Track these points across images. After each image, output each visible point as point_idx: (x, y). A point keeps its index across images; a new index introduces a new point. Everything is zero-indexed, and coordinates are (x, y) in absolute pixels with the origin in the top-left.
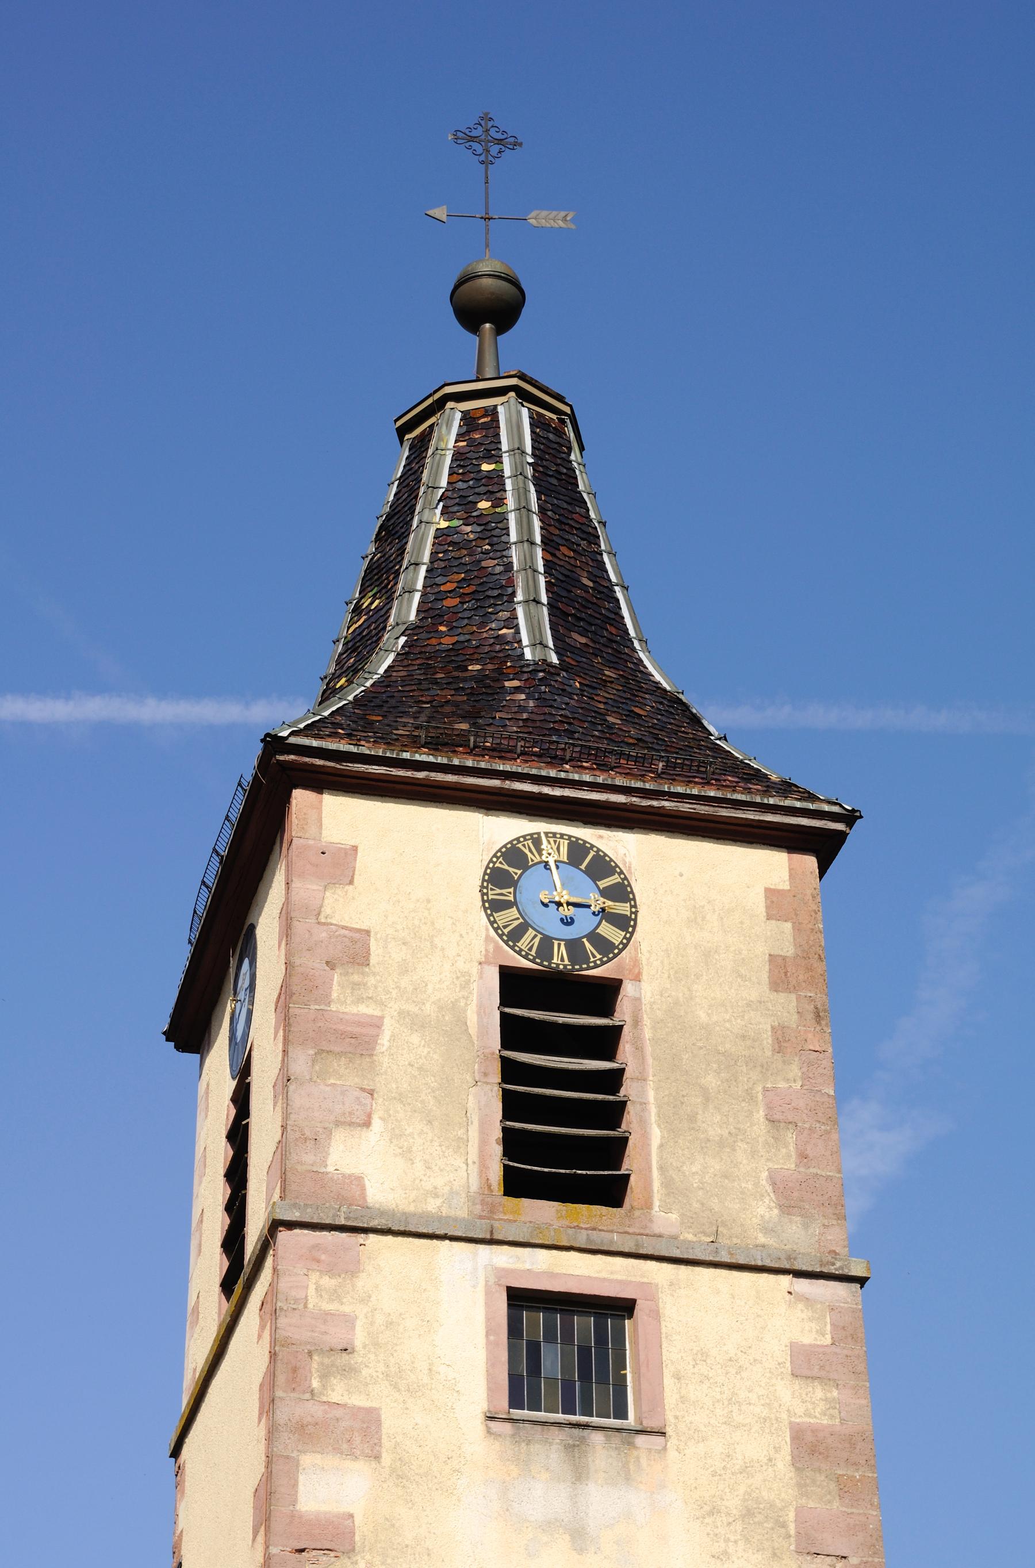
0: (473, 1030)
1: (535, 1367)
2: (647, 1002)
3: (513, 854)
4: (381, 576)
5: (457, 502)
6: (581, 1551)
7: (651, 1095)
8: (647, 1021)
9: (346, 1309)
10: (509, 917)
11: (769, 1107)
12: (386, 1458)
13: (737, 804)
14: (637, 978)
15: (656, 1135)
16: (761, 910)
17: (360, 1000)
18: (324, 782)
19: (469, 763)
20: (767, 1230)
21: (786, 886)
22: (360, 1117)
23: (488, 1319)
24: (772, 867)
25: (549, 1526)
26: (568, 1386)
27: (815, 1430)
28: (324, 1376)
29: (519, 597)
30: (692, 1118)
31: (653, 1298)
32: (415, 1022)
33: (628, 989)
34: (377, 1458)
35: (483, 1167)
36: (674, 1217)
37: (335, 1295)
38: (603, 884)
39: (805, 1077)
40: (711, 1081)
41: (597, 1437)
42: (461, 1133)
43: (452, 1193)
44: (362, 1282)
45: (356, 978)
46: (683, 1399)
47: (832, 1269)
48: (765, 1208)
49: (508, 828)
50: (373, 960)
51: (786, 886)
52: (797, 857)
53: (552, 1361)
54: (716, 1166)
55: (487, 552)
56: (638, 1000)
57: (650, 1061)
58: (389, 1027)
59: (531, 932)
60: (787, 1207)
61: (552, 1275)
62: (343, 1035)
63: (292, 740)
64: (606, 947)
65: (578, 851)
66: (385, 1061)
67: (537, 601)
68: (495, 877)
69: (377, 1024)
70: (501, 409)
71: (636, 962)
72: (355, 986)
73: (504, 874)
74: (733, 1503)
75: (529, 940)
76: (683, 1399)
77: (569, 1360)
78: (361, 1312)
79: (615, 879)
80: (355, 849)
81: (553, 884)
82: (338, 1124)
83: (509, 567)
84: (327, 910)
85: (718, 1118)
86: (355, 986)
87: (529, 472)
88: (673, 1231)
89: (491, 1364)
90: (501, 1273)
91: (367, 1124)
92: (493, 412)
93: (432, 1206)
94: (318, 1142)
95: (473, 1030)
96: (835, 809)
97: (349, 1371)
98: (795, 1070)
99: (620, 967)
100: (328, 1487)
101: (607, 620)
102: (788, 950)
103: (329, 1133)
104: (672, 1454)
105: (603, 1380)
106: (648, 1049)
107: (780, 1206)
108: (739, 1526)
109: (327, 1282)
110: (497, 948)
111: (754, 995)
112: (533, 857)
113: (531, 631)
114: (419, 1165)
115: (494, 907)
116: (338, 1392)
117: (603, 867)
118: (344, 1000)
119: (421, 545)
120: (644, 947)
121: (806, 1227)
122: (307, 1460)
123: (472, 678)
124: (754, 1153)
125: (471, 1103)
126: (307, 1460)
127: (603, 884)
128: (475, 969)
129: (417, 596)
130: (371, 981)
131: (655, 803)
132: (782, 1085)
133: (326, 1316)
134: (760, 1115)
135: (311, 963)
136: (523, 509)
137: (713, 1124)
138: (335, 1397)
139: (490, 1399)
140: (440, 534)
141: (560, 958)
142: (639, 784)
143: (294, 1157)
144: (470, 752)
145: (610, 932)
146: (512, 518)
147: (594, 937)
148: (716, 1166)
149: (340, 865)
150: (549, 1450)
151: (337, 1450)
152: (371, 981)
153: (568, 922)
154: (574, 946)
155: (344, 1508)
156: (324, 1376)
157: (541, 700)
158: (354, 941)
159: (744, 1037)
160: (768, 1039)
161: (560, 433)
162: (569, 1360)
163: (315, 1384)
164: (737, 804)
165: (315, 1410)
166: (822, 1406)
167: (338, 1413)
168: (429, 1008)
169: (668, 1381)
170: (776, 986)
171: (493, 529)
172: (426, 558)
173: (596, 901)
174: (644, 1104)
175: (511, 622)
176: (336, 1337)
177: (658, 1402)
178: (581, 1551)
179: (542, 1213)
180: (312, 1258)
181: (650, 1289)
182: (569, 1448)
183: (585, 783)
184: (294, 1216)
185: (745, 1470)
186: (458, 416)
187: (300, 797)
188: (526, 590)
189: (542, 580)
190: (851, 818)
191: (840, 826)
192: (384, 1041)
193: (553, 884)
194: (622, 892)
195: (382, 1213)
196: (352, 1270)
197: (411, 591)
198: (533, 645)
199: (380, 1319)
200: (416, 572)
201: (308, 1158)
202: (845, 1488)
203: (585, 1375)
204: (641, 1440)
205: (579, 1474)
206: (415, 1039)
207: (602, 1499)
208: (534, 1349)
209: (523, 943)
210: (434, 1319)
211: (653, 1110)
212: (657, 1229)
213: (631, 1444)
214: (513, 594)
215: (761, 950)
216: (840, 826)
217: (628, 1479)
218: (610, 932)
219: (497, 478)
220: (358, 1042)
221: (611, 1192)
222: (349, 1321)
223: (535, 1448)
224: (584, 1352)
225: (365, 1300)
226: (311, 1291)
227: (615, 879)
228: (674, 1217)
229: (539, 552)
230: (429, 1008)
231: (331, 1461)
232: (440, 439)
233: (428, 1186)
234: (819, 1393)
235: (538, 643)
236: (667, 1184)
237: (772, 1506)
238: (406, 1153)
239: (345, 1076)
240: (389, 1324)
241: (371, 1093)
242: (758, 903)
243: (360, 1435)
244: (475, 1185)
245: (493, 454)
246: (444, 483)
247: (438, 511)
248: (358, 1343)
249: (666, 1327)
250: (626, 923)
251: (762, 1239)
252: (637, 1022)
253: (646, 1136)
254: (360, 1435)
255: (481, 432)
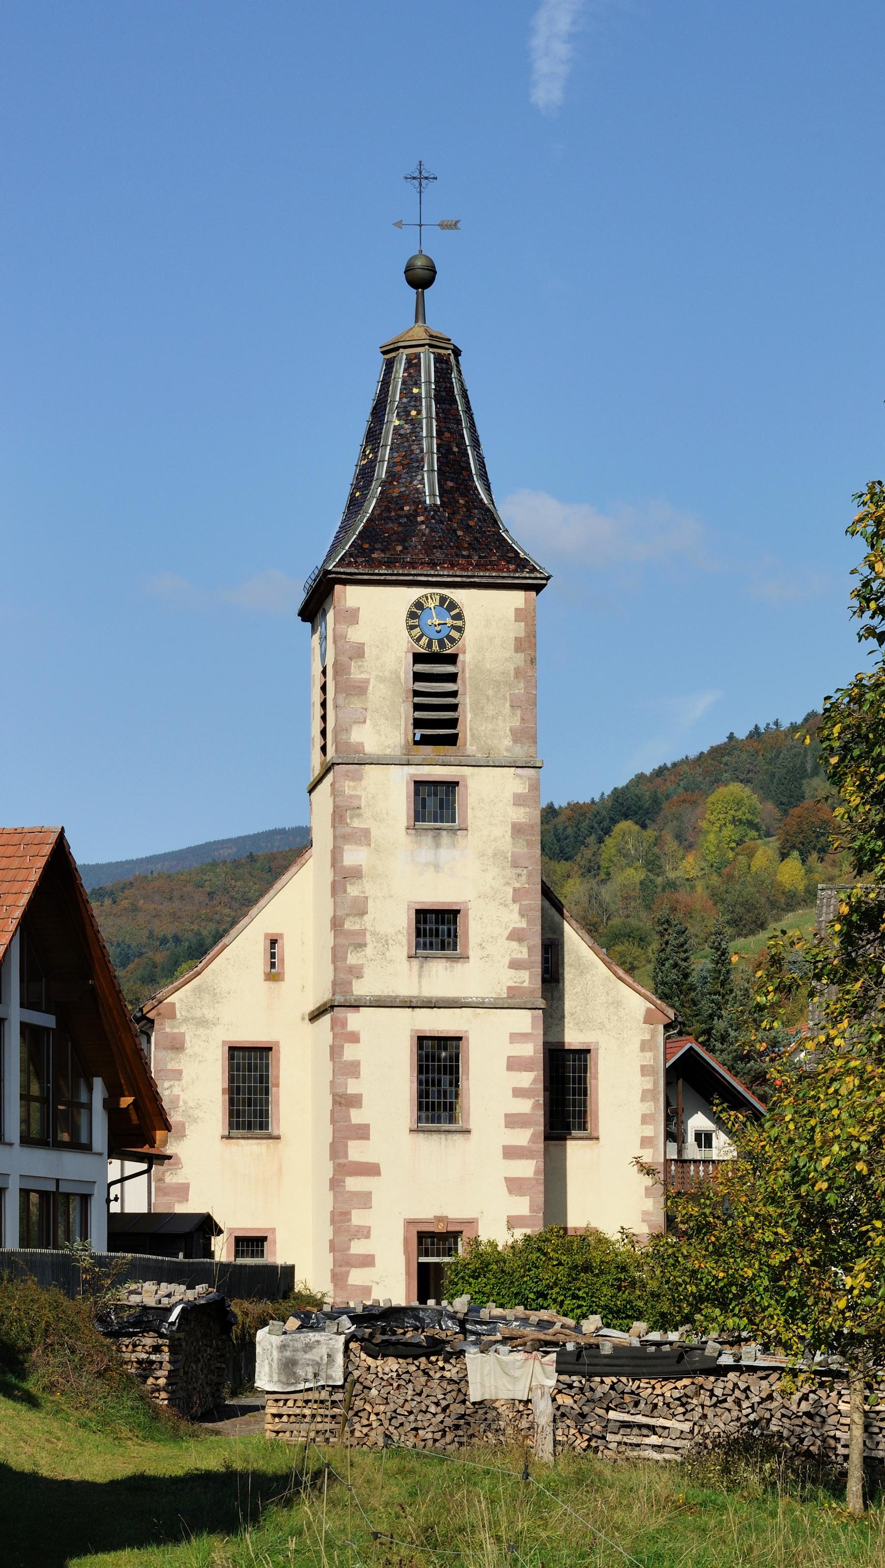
0: (403, 681)
1: (424, 807)
2: (468, 659)
3: (418, 605)
4: (373, 436)
5: (404, 413)
6: (437, 872)
7: (468, 700)
8: (467, 670)
9: (358, 793)
10: (416, 632)
11: (511, 701)
12: (373, 845)
13: (503, 577)
14: (464, 653)
15: (469, 716)
16: (513, 618)
17: (362, 672)
18: (345, 582)
19: (401, 572)
20: (507, 750)
21: (523, 606)
22: (362, 720)
23: (407, 793)
24: (518, 598)
25: (427, 864)
26: (435, 813)
27: (520, 824)
28: (351, 818)
29: (426, 469)
30: (482, 709)
31: (465, 780)
32: (381, 679)
33: (461, 658)
34: (370, 845)
35: (406, 735)
36: (474, 748)
37: (355, 788)
38: (453, 613)
39: (525, 688)
40: (490, 692)
41: (444, 833)
42: (398, 722)
43: (395, 746)
44: (364, 783)
45: (360, 663)
46: (474, 817)
47: (530, 765)
48: (507, 742)
49: (416, 593)
50: (366, 655)
51: (523, 606)
52: (528, 593)
53: (431, 802)
54: (490, 726)
55: (414, 441)
56: (464, 661)
57: (468, 686)
58: (372, 682)
59: (424, 637)
60: (515, 741)
61: (430, 775)
62: (355, 687)
63: (334, 570)
64: (452, 640)
65: (443, 599)
66: (371, 696)
67: (433, 471)
68: (412, 615)
69: (367, 681)
70: (422, 355)
71: (464, 645)
72: (360, 666)
73: (416, 611)
74: (490, 852)
75: (424, 641)
76: (474, 817)
77: (435, 804)
78: (363, 794)
79: (457, 611)
80: (359, 608)
81: (434, 619)
82: (355, 722)
83: (422, 451)
84: (349, 636)
85: (492, 707)
86: (360, 666)
87: (433, 392)
88: (474, 753)
89: (408, 809)
90: (412, 775)
91: (365, 722)
92: (417, 356)
93: (388, 751)
94: (347, 730)
95: (403, 681)
96: (542, 576)
97: (359, 816)
98: (522, 685)
99: (458, 648)
100: (353, 856)
101: (463, 468)
102: (522, 634)
103: (351, 726)
104: (469, 836)
105: (448, 809)
106: (467, 682)
107: (513, 740)
108: (491, 860)
109: (352, 784)
110: (412, 645)
111: (508, 655)
112: (426, 605)
113: (429, 487)
114: (383, 736)
115: (411, 628)
116: (356, 823)
117: (453, 605)
118: (356, 674)
119: (388, 437)
120: (467, 639)
121: (522, 747)
122: (346, 847)
123: (406, 516)
124: (504, 720)
125: (402, 710)
126: (346, 847)
127: (453, 613)
128: (403, 655)
129: (386, 463)
130: (365, 664)
131: (472, 580)
132: (517, 691)
133: (351, 796)
134: (508, 704)
135: (344, 659)
136: (429, 418)
137: (490, 710)
138: (355, 825)
139: (278, 1093)
140: (395, 428)
141: (436, 648)
142: (466, 574)
143: (339, 737)
144: (403, 566)
145: (454, 634)
146: (424, 421)
147: (449, 637)
148: (490, 726)
149: (352, 616)
150: (428, 839)
151: (356, 843)
152: (365, 664)
153: (439, 632)
154: (441, 643)
155: (359, 863)
156: (351, 818)
157: (432, 530)
158: (359, 648)
159: (503, 673)
160: (512, 673)
161: (447, 362)
162: (435, 804)
163: (348, 821)
164: (503, 577)
165: (348, 830)
166: (523, 815)
167: (356, 830)
168: (387, 673)
169: (469, 811)
170: (517, 650)
171: (415, 424)
172: (389, 443)
173: (449, 621)
174: (465, 704)
175: (422, 481)
176: (355, 803)
177: (465, 819)
178: (437, 872)
179: (428, 750)
180: (346, 775)
181: (464, 777)
182: (434, 837)
183: (444, 574)
184: (340, 761)
185: (495, 840)
186: (404, 357)
187: (338, 588)
188: (428, 464)
189: (435, 456)
190: (548, 578)
191: (544, 582)
192: (370, 688)
193: (434, 619)
194: (459, 617)
195: (370, 758)
196: (358, 778)
197: (386, 446)
198: (430, 495)
199: (370, 796)
200: (386, 449)
201: (344, 737)
202: (529, 844)
203: (441, 808)
204: (459, 832)
205: (438, 846)
206: (382, 686)
207: (445, 853)
208: (424, 800)
209: (421, 643)
210: (388, 794)
211: (468, 706)
212: (468, 754)
213: (456, 834)
214: (423, 467)
215: (512, 635)
216: (544, 582)
217: (454, 846)
218: (454, 634)
219: (418, 398)
220: (361, 689)
221: (452, 740)
222: (359, 797)
223: (423, 838)
224: (441, 800)
225: (365, 789)
226: (346, 788)
227: (457, 611)
228: (474, 748)
229: (435, 441)
230: (387, 673)
231: (354, 847)
232: (396, 371)
233: (386, 744)
234: (522, 810)
235: (432, 495)
236: (472, 735)
237: (503, 851)
238: (379, 733)
239: (356, 703)
240: (373, 797)
241: (366, 709)
242: (512, 615)
243: (364, 837)
244: (403, 742)
245: (417, 384)
246: (397, 399)
247: (395, 415)
248: (362, 805)
249: (469, 790)
250: (460, 629)
251: (506, 754)
252: (463, 671)
253: (465, 717)
254: (364, 837)
255: (413, 364)
